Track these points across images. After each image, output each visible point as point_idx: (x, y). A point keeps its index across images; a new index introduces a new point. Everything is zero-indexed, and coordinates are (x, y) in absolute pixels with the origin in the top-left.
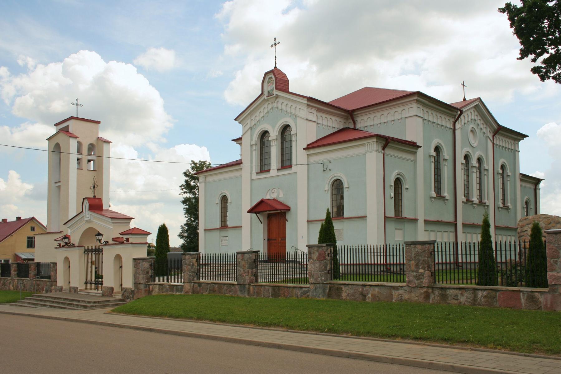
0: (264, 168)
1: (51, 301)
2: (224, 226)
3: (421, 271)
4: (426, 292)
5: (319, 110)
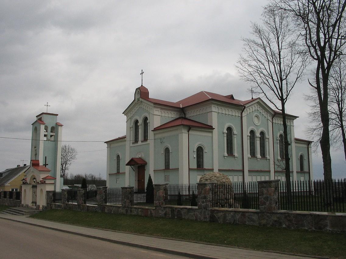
0: (136, 141)
1: (14, 211)
2: (118, 172)
3: (125, 200)
4: (127, 209)
5: (161, 109)
